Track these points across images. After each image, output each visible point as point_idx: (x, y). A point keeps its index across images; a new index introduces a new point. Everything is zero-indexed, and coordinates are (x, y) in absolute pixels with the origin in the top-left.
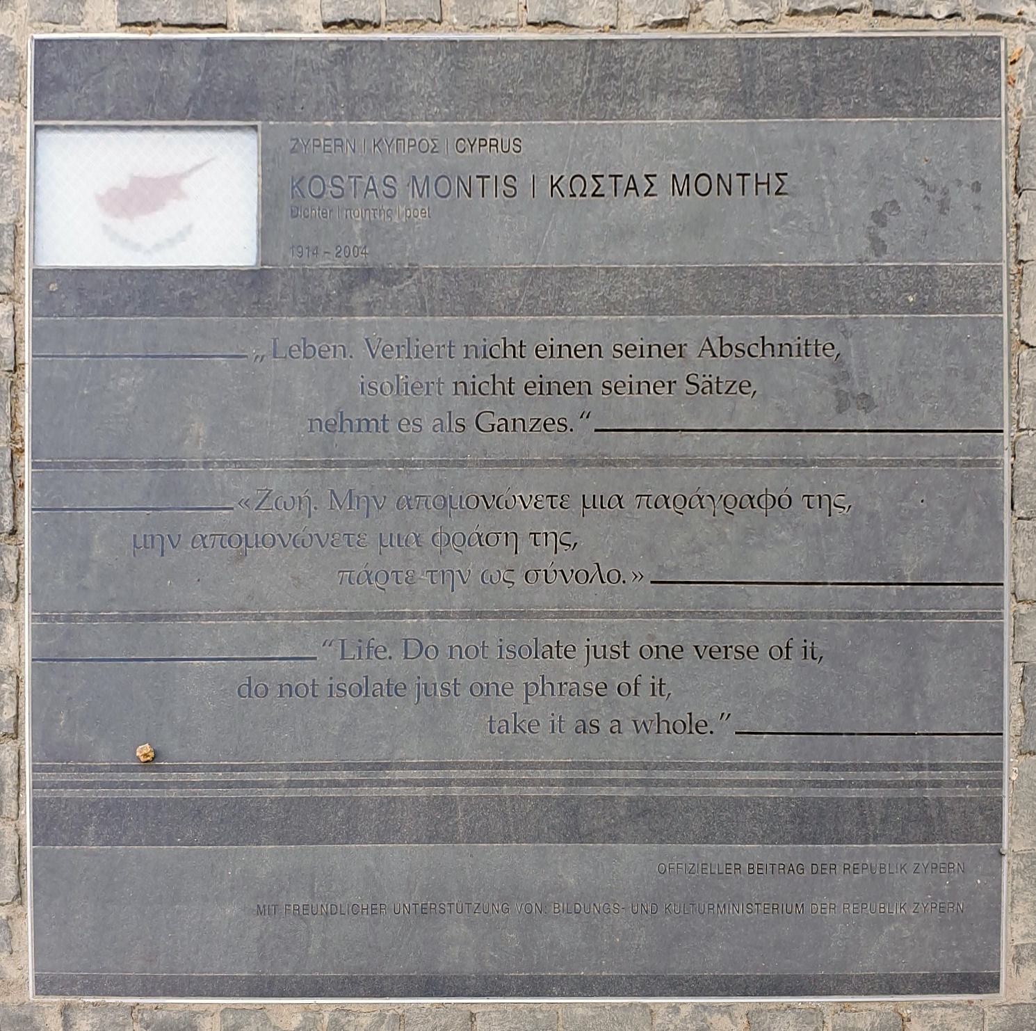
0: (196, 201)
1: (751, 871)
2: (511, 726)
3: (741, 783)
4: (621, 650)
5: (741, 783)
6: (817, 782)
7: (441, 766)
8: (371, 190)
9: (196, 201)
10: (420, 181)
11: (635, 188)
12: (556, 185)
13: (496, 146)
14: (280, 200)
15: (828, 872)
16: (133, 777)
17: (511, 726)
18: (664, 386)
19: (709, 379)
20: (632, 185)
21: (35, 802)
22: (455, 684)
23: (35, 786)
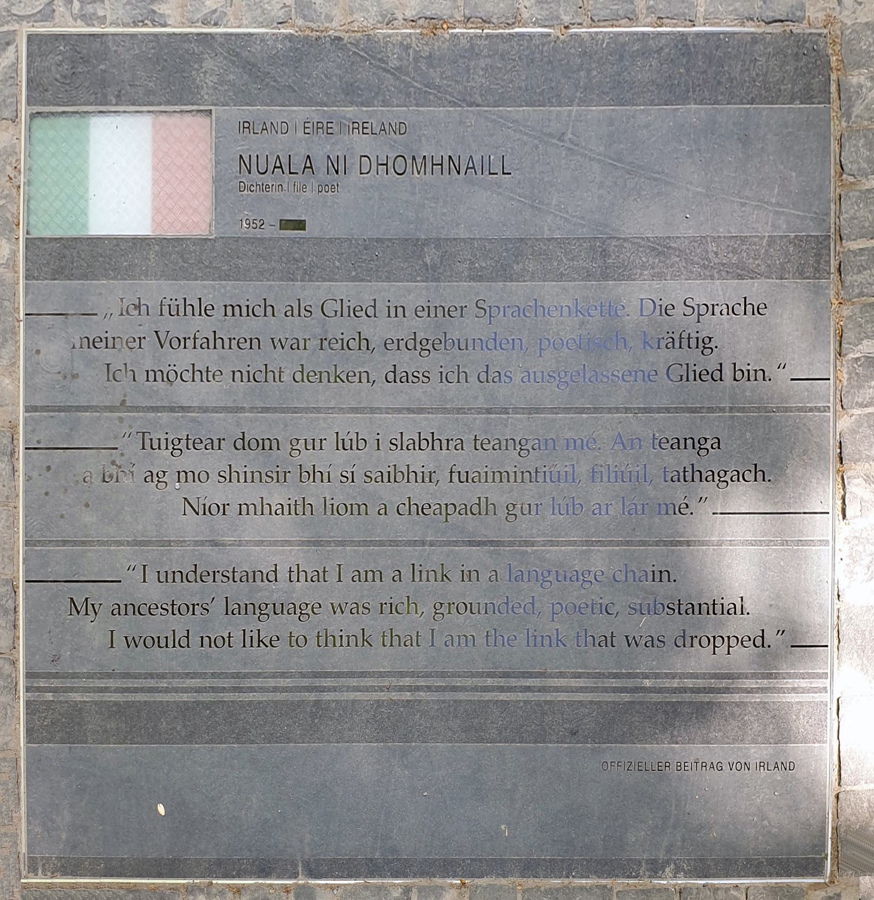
0: (126, 176)
1: (679, 768)
2: (554, 641)
3: (605, 690)
4: (230, 575)
5: (605, 690)
6: (749, 692)
7: (316, 675)
8: (471, 168)
9: (126, 176)
10: (419, 160)
11: (311, 167)
13: (322, 128)
14: (242, 172)
15: (663, 768)
16: (184, 683)
17: (554, 641)
18: (101, 341)
19: (672, 336)
20: (278, 165)
21: (28, 703)
22: (679, 604)
23: (28, 690)
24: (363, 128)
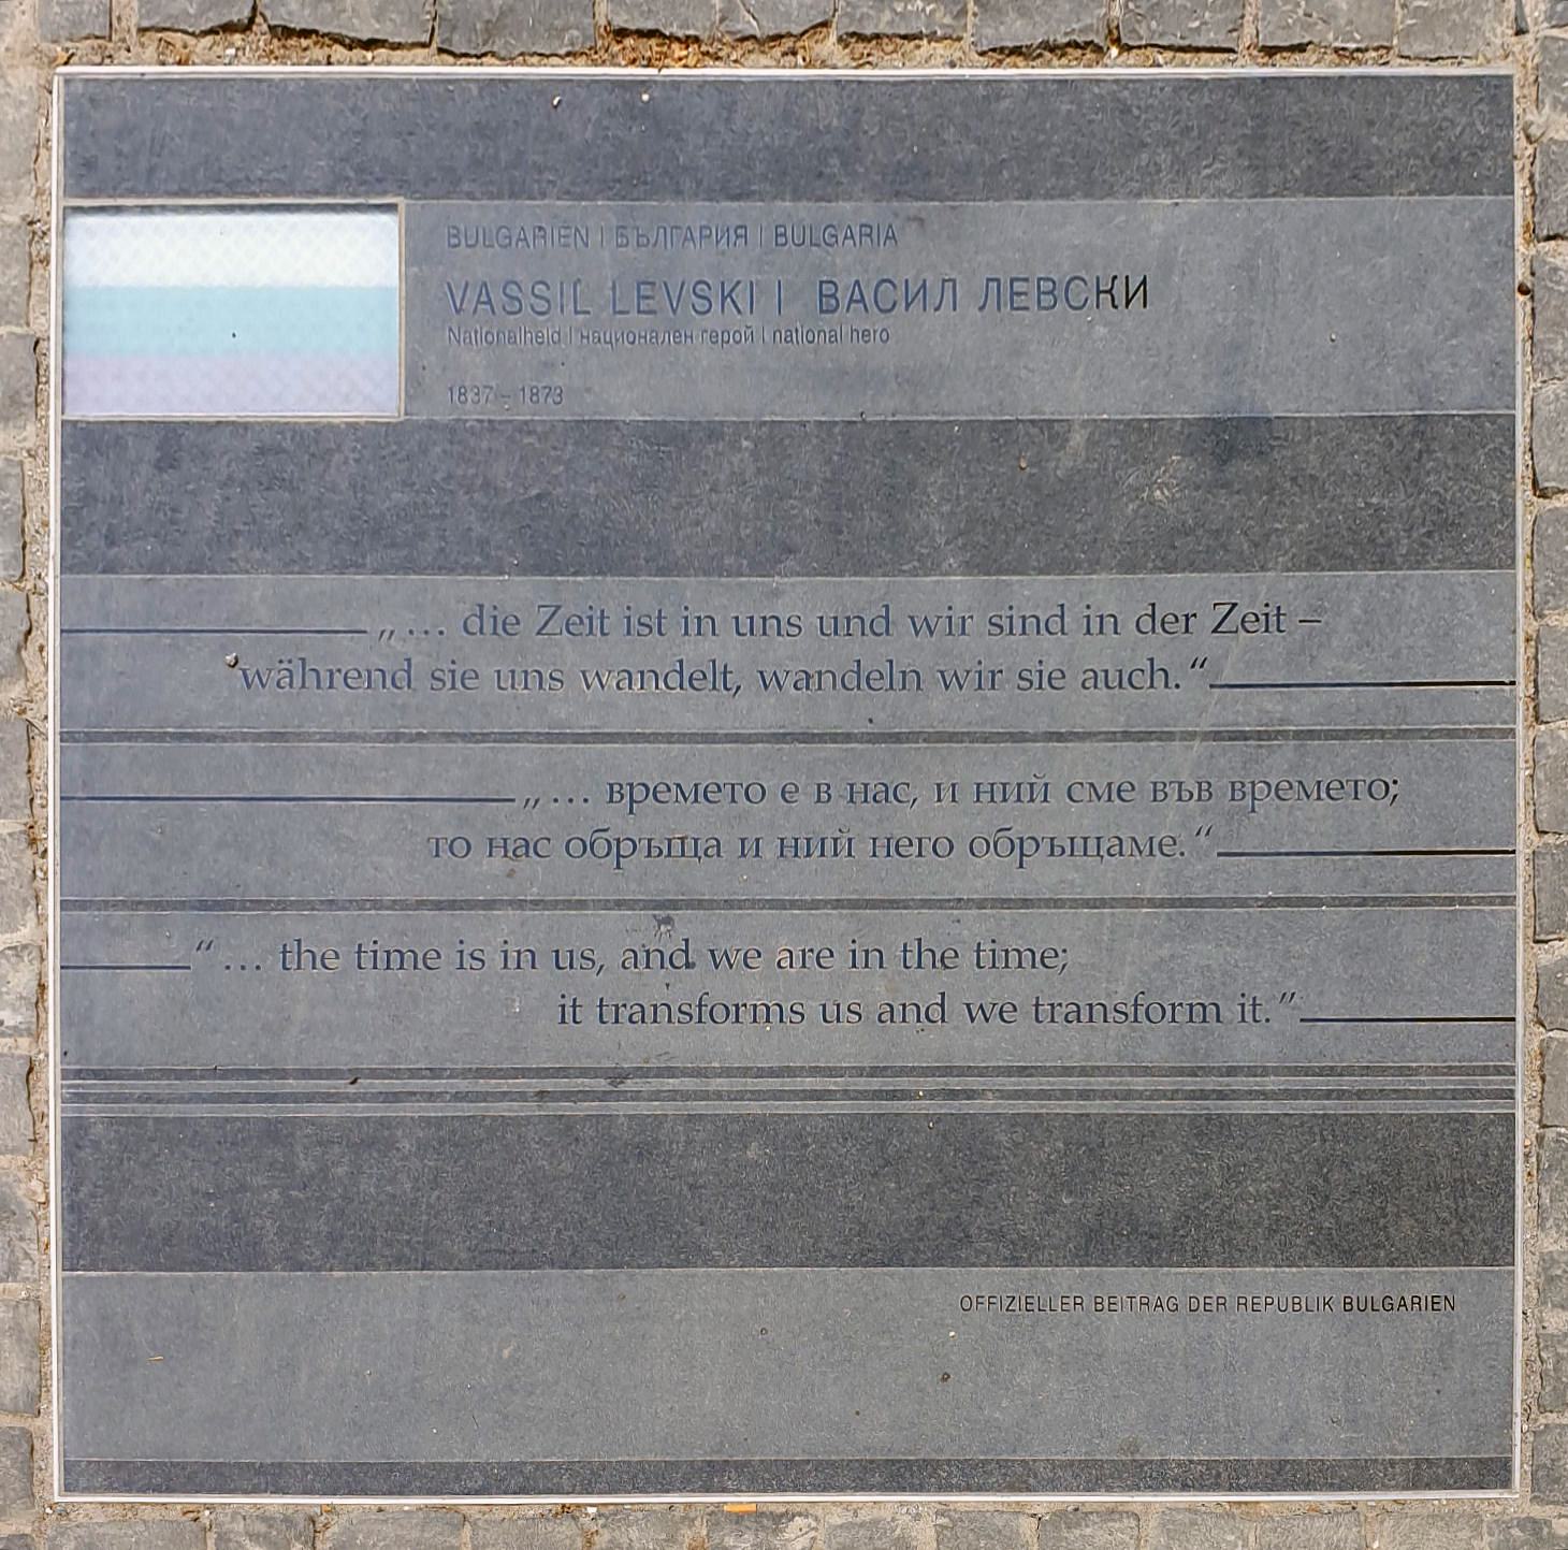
12: (730, 295)
20: (857, 296)
24: (1013, 293)
